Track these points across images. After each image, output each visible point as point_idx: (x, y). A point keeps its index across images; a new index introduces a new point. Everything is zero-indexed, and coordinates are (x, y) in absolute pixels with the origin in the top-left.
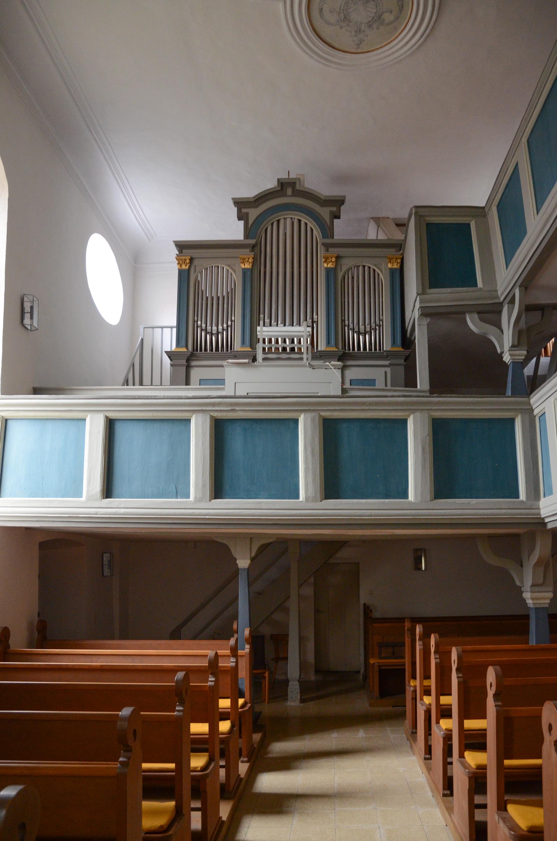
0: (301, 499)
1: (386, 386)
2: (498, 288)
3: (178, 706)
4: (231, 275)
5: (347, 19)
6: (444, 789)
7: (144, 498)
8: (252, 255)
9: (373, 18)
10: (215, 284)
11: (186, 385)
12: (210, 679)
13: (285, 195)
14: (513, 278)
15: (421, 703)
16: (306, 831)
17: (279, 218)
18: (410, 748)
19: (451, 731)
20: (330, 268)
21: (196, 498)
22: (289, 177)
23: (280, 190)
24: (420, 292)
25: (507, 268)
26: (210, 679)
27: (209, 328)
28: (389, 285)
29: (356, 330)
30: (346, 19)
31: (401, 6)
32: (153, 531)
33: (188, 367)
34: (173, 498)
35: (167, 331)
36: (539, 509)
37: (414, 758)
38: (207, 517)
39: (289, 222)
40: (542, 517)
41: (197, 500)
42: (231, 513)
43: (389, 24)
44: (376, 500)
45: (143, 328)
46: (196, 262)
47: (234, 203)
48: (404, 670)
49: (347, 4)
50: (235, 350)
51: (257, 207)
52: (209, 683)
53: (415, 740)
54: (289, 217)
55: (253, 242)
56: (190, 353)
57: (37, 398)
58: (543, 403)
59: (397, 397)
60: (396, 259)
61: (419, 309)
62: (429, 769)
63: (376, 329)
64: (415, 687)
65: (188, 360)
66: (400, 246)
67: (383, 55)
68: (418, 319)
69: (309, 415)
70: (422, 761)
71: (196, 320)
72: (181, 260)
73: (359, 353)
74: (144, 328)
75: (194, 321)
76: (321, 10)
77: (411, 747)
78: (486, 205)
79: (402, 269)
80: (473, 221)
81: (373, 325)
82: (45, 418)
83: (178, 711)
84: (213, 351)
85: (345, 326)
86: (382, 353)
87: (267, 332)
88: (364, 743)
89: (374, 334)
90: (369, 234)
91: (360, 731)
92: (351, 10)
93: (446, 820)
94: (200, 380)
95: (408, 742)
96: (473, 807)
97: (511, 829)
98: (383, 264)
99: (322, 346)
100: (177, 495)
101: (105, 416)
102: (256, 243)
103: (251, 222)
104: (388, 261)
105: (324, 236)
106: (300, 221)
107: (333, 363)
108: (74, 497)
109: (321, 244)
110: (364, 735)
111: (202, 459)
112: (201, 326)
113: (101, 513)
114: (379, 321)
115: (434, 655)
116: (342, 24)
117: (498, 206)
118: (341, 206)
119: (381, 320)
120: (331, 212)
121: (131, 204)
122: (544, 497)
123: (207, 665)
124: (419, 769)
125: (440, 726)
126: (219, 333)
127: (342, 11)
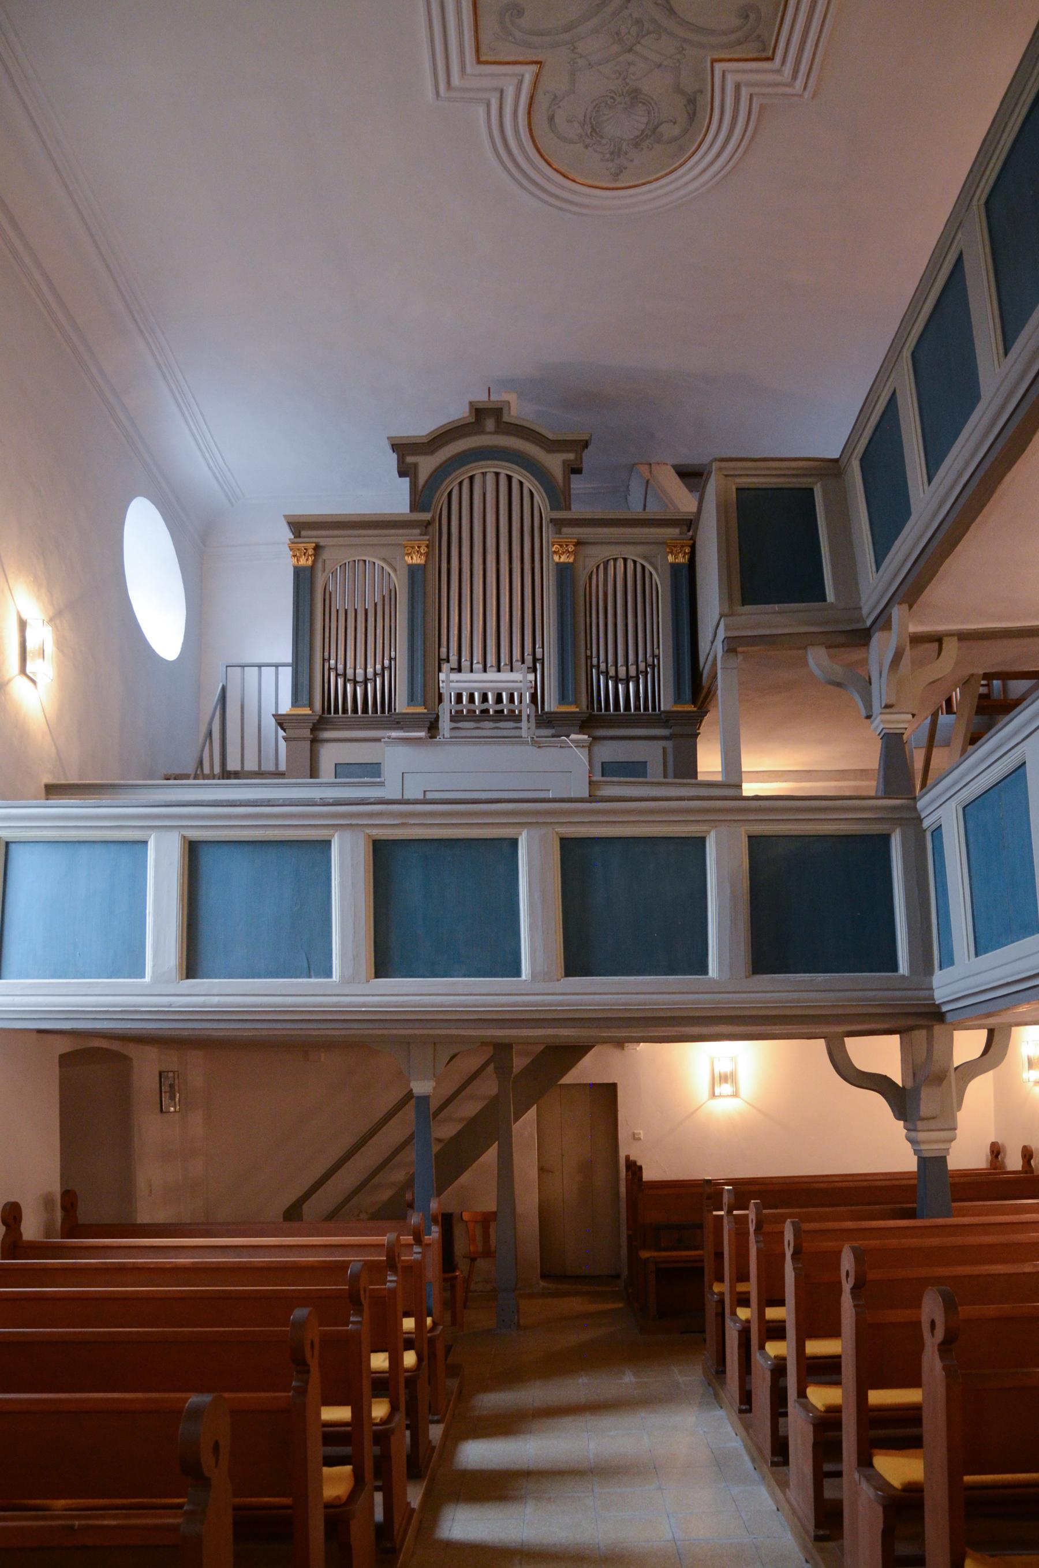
0: (524, 977)
1: (665, 776)
2: (862, 604)
3: (354, 1315)
4: (380, 571)
5: (596, 132)
6: (773, 1454)
7: (253, 977)
8: (424, 540)
9: (643, 131)
10: (351, 580)
11: (311, 777)
12: (389, 1278)
13: (482, 432)
14: (886, 590)
15: (732, 1320)
16: (548, 1524)
17: (474, 473)
18: (713, 1397)
19: (784, 1359)
20: (564, 563)
21: (342, 976)
22: (489, 399)
23: (473, 423)
24: (726, 611)
25: (877, 571)
26: (389, 1278)
27: (350, 672)
28: (669, 594)
29: (612, 673)
30: (596, 132)
31: (691, 112)
32: (265, 1033)
33: (315, 741)
34: (303, 978)
35: (268, 673)
36: (931, 989)
37: (721, 1413)
38: (363, 1009)
39: (490, 479)
40: (937, 1002)
41: (345, 980)
42: (403, 1002)
43: (670, 142)
44: (652, 977)
45: (225, 667)
46: (326, 555)
47: (393, 445)
48: (703, 1268)
49: (596, 109)
50: (397, 711)
51: (432, 453)
52: (388, 1284)
53: (723, 1383)
54: (490, 472)
55: (426, 516)
56: (317, 718)
57: (61, 805)
58: (938, 810)
59: (688, 800)
60: (682, 546)
61: (723, 642)
62: (747, 1427)
63: (647, 673)
64: (722, 1294)
65: (313, 730)
66: (690, 524)
67: (660, 192)
68: (722, 658)
69: (537, 832)
70: (735, 1417)
71: (326, 657)
72: (299, 550)
73: (617, 715)
74: (227, 666)
75: (324, 660)
76: (551, 119)
77: (716, 1396)
78: (841, 456)
79: (692, 564)
80: (819, 485)
81: (642, 666)
82: (76, 840)
83: (353, 1323)
84: (358, 713)
85: (592, 666)
86: (658, 715)
87: (457, 682)
88: (635, 1392)
89: (643, 682)
90: (630, 493)
91: (626, 1372)
92: (605, 118)
93: (776, 1501)
94: (336, 764)
95: (710, 1388)
96: (820, 1476)
97: (877, 1489)
98: (659, 557)
99: (551, 704)
100: (310, 972)
101: (182, 835)
102: (433, 518)
103: (422, 478)
104: (668, 550)
105: (555, 506)
106: (509, 478)
107: (573, 736)
108: (130, 977)
109: (548, 520)
110: (633, 1380)
111: (353, 908)
112: (336, 669)
113: (178, 1004)
114: (651, 658)
115: (755, 1237)
116: (588, 141)
117: (862, 460)
118: (583, 450)
119: (656, 656)
120: (564, 462)
121: (200, 441)
122: (941, 970)
123: (385, 1258)
124: (730, 1428)
125: (767, 1353)
126: (368, 681)
127: (587, 120)
